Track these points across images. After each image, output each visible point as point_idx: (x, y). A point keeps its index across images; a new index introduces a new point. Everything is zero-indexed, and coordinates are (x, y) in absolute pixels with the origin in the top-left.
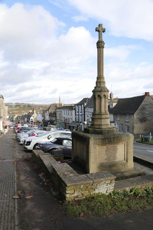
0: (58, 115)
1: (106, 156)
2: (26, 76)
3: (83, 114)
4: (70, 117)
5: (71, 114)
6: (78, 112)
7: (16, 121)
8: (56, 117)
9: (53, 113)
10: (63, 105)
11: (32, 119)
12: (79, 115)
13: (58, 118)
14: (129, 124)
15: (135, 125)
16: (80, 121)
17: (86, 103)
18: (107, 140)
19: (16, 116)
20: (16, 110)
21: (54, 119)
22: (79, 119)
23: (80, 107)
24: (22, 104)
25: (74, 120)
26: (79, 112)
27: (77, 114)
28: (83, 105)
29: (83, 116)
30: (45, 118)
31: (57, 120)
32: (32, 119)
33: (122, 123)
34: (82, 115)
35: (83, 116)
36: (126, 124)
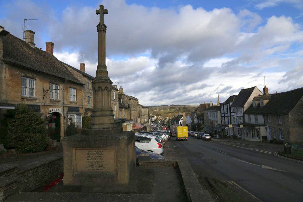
0: (205, 118)
1: (88, 163)
2: (204, 74)
3: (229, 115)
4: (215, 119)
5: (216, 116)
6: (224, 113)
7: (167, 125)
8: (204, 119)
9: (200, 115)
10: (211, 105)
11: (181, 123)
12: (224, 117)
13: (205, 121)
14: (283, 128)
15: (291, 129)
16: (227, 124)
17: (232, 101)
18: (85, 143)
19: (168, 119)
20: (170, 113)
21: (201, 122)
22: (225, 120)
23: (225, 106)
24: (178, 106)
25: (220, 122)
26: (225, 114)
27: (223, 115)
28: (228, 104)
29: (229, 117)
30: (193, 121)
31: (205, 124)
32: (181, 123)
33: (275, 126)
34: (228, 116)
35: (229, 117)
36: (279, 127)
